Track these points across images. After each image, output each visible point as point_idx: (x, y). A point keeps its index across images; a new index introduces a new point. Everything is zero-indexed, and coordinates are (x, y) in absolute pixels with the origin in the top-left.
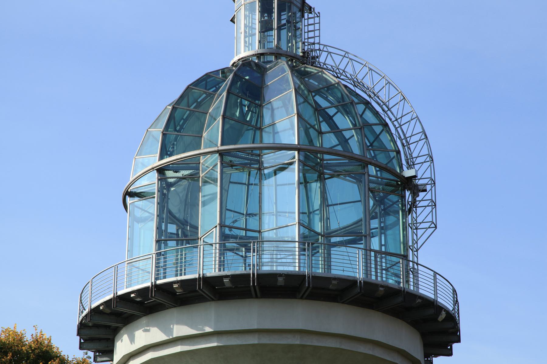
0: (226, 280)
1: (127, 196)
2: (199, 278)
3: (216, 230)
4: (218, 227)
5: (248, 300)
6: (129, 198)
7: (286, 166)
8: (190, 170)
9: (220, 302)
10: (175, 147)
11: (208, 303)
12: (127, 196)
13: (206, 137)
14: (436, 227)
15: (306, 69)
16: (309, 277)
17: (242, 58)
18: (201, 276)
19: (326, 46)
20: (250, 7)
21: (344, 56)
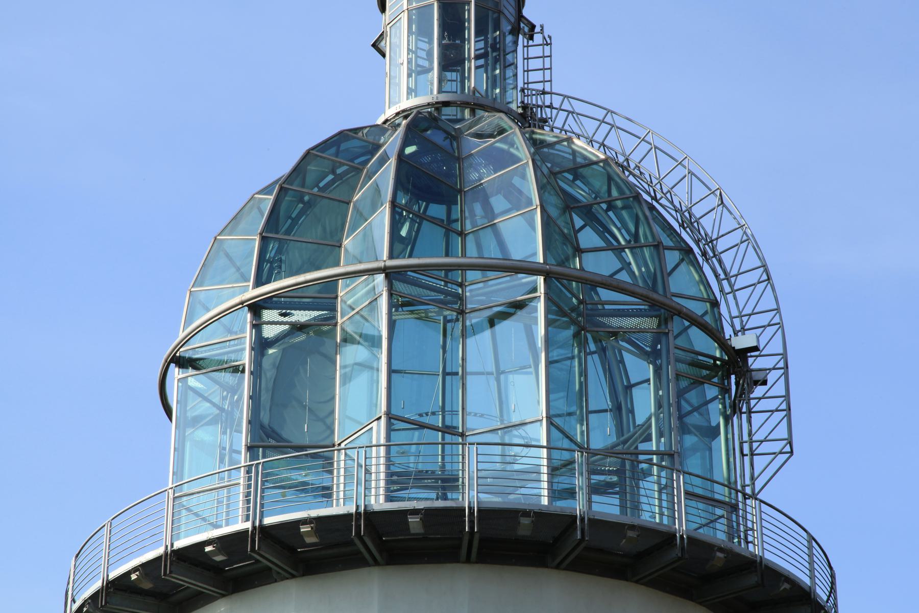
0: (412, 519)
1: (173, 365)
2: (358, 514)
3: (379, 426)
4: (383, 421)
5: (449, 566)
6: (177, 369)
7: (512, 310)
8: (318, 310)
9: (390, 569)
10: (283, 266)
11: (364, 572)
12: (173, 365)
13: (350, 248)
14: (792, 452)
15: (534, 136)
16: (582, 519)
17: (403, 111)
18: (362, 509)
19: (569, 97)
20: (419, 18)
21: (603, 121)
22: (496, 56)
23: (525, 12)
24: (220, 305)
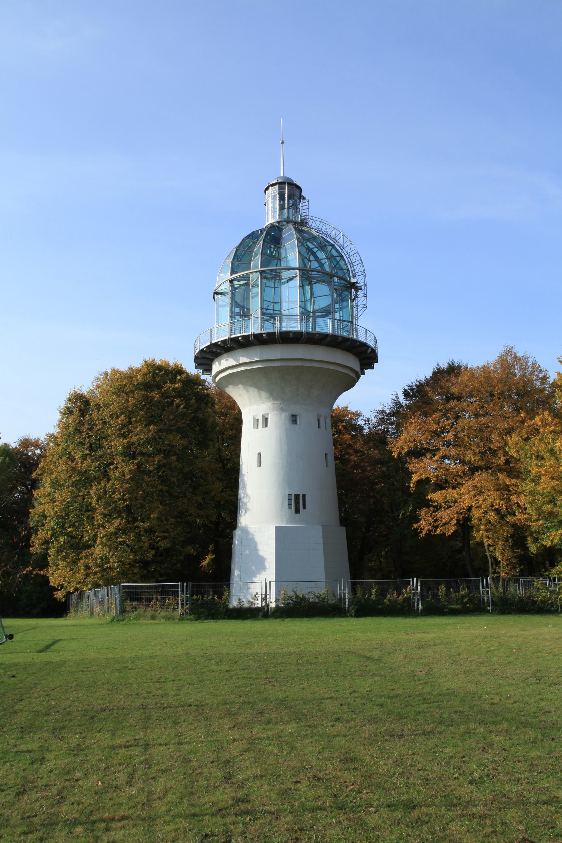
22: (295, 207)
23: (302, 194)
24: (222, 279)
